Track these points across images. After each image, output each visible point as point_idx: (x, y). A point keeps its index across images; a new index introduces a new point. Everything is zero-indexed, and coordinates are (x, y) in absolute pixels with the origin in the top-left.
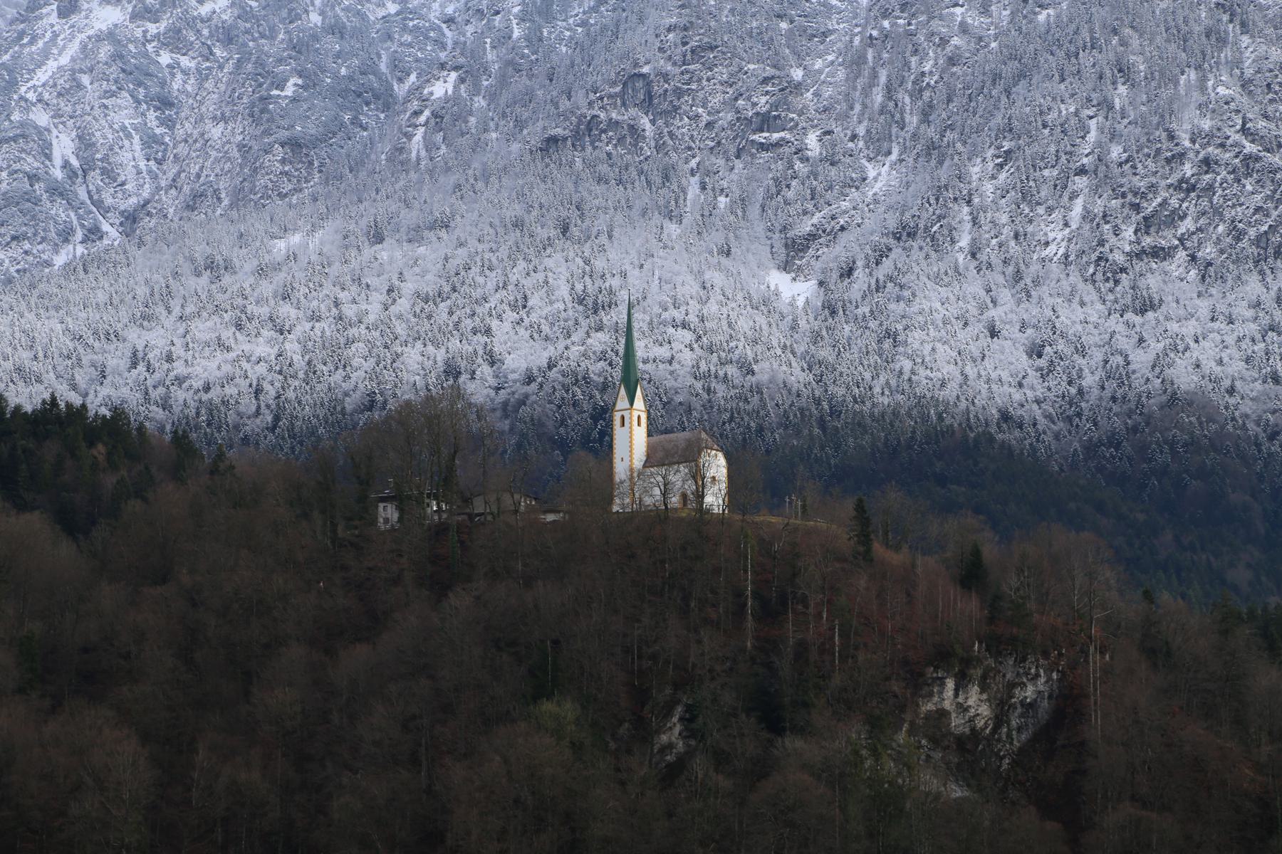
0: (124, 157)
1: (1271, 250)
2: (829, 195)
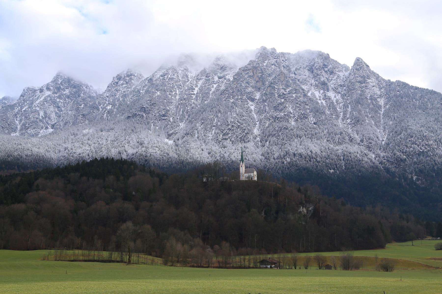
0: (52, 116)
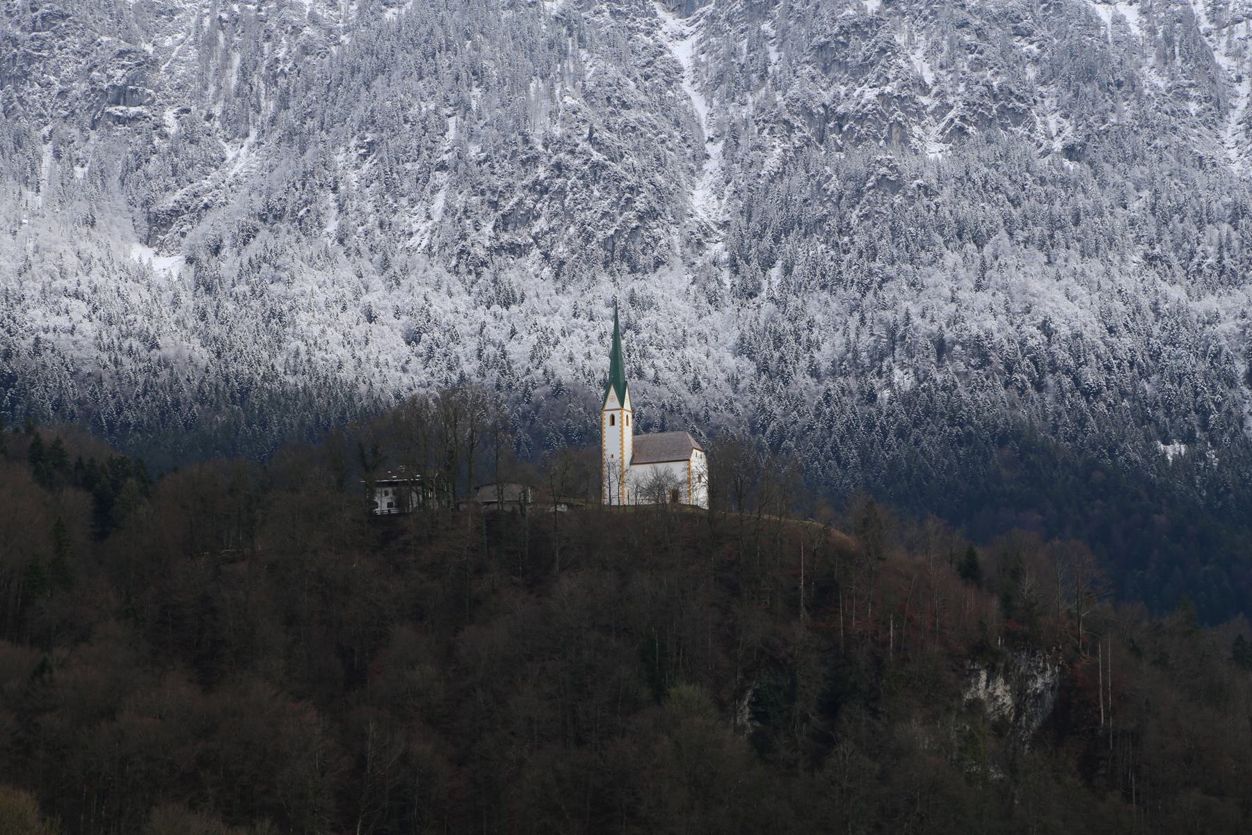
1: (617, 253)
2: (190, 173)
